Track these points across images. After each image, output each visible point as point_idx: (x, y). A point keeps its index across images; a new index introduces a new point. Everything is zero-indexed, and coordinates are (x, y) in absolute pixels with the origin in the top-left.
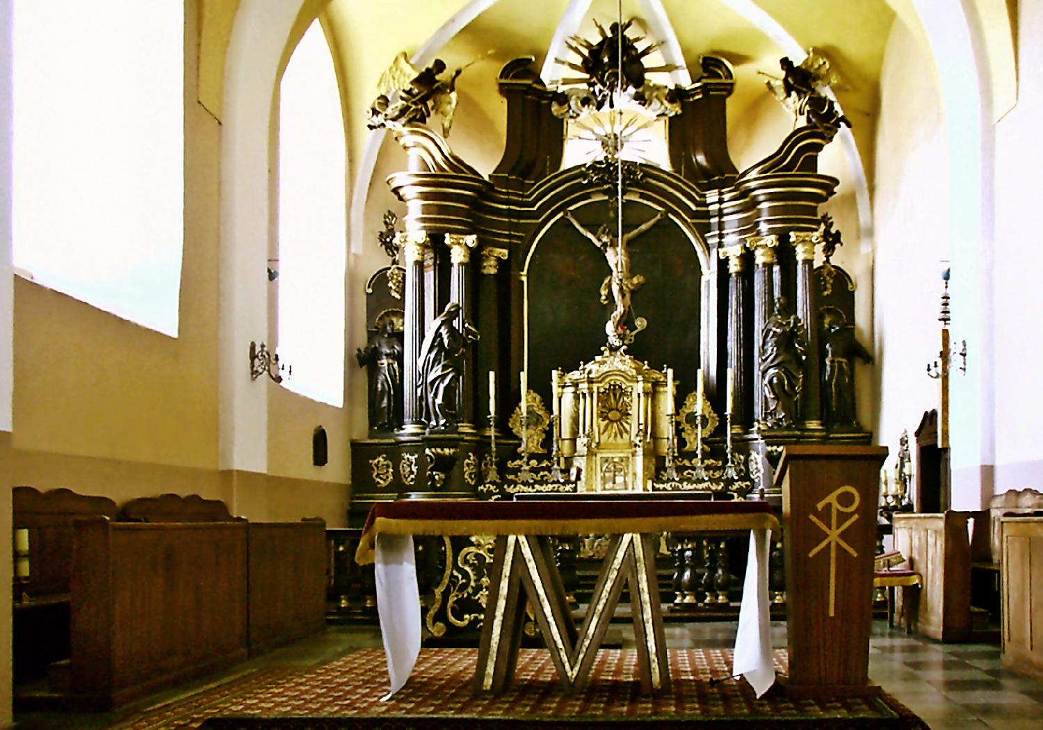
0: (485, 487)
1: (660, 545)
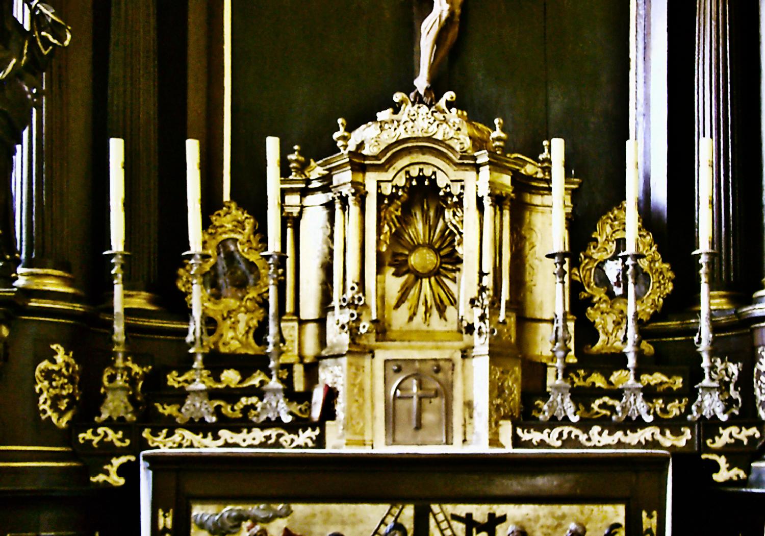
0: (95, 434)
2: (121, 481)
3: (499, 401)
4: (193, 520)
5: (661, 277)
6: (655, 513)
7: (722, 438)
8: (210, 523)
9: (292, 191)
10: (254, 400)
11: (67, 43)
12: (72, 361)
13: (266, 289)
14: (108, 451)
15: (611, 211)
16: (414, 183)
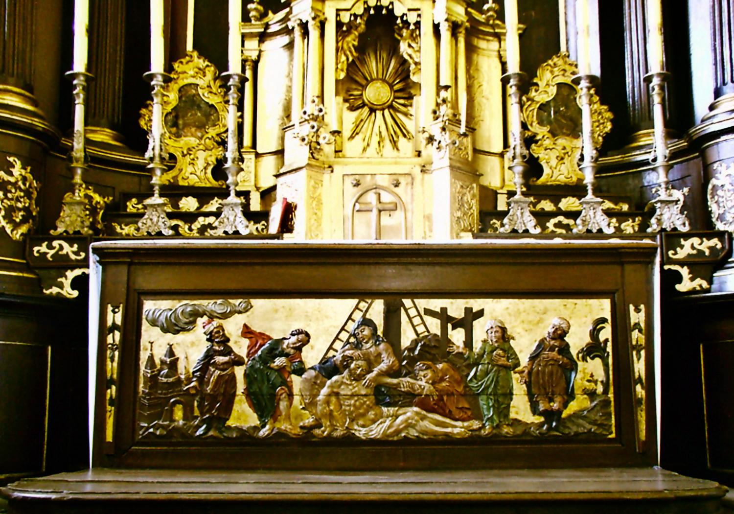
0: (50, 247)
1: (509, 395)
2: (75, 294)
3: (459, 214)
4: (144, 317)
5: (600, 117)
6: (642, 307)
7: (684, 248)
8: (162, 319)
9: (252, 35)
10: (211, 220)
12: (30, 176)
13: (225, 129)
14: (63, 264)
15: (550, 58)
16: (372, 12)
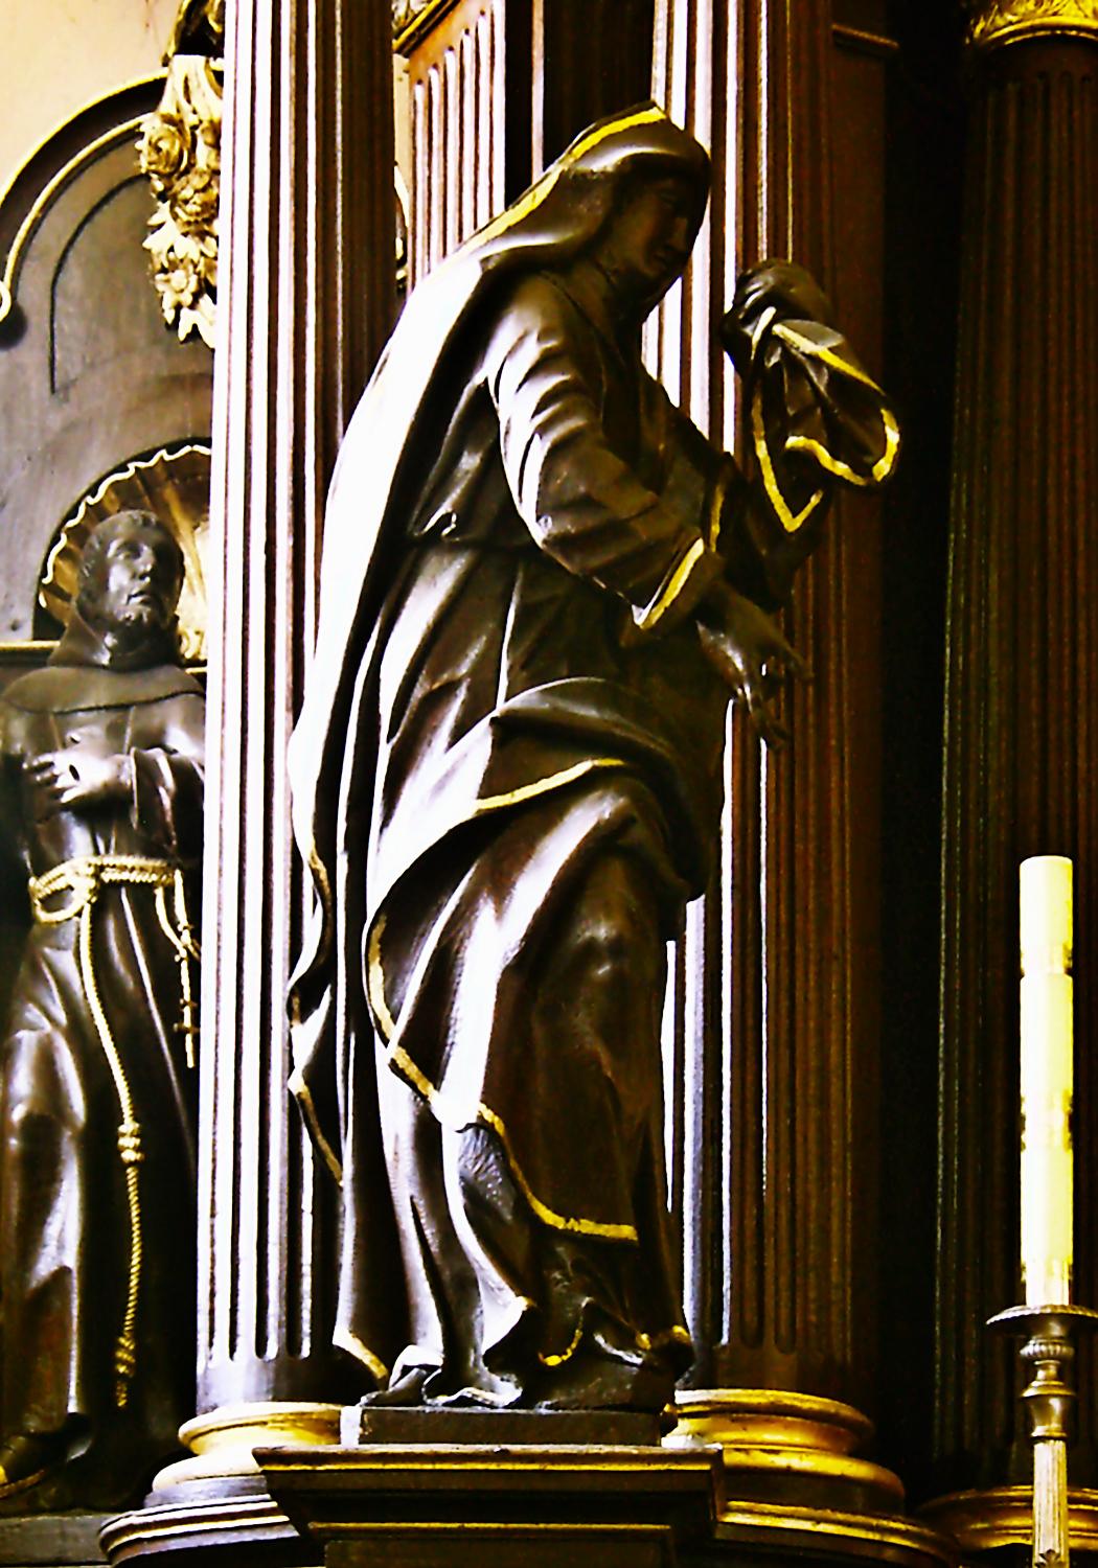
11: (883, 468)
